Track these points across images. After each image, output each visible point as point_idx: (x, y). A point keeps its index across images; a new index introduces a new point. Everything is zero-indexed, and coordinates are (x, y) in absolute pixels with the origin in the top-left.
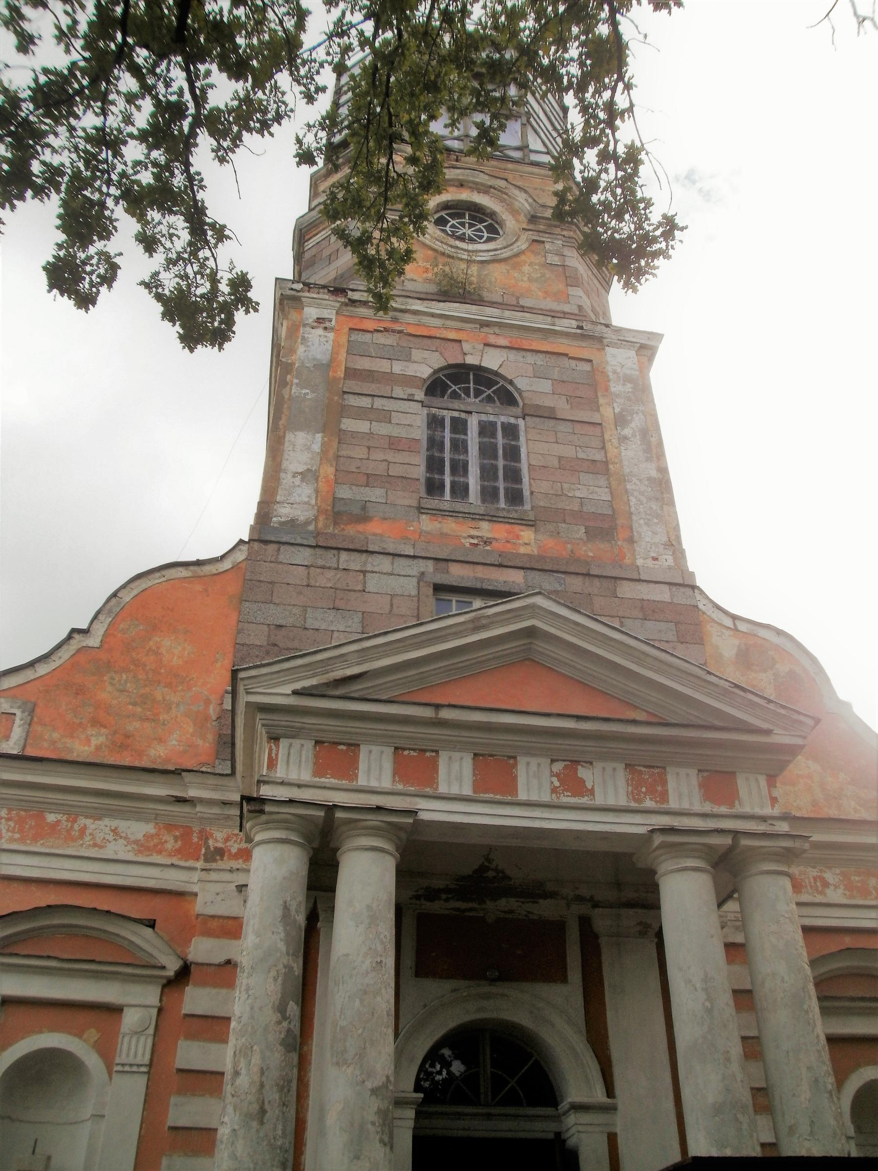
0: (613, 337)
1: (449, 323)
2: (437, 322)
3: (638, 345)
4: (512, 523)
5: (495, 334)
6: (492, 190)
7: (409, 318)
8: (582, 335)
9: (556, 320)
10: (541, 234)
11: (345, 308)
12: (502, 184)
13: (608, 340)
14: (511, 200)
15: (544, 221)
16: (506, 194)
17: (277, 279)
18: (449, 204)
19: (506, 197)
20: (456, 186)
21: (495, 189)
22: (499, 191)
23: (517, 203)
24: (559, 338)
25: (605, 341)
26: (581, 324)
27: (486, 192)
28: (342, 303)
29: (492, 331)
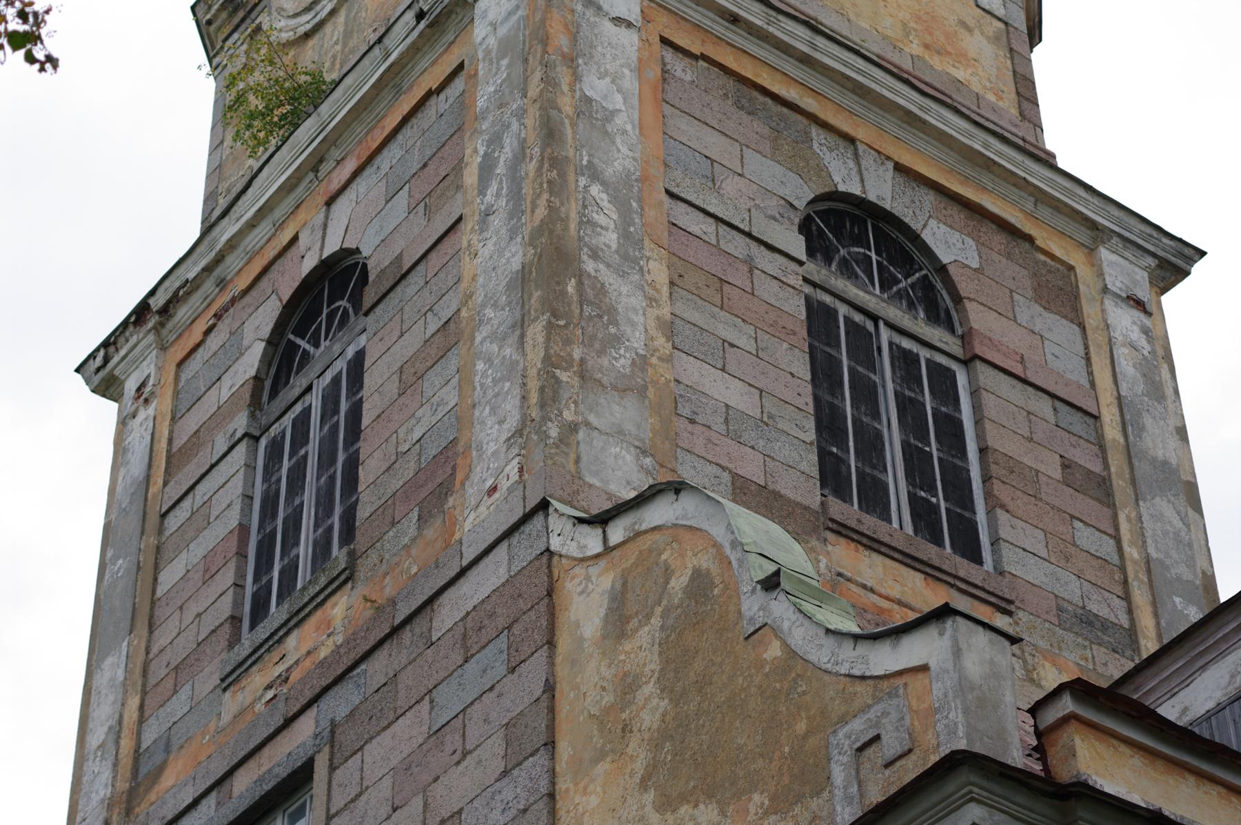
1: (279, 213)
2: (264, 229)
4: (983, 589)
5: (338, 162)
7: (233, 262)
8: (430, 26)
9: (386, 40)
11: (164, 332)
17: (77, 370)
20: (980, 167)
26: (416, 8)
28: (154, 328)
29: (332, 164)
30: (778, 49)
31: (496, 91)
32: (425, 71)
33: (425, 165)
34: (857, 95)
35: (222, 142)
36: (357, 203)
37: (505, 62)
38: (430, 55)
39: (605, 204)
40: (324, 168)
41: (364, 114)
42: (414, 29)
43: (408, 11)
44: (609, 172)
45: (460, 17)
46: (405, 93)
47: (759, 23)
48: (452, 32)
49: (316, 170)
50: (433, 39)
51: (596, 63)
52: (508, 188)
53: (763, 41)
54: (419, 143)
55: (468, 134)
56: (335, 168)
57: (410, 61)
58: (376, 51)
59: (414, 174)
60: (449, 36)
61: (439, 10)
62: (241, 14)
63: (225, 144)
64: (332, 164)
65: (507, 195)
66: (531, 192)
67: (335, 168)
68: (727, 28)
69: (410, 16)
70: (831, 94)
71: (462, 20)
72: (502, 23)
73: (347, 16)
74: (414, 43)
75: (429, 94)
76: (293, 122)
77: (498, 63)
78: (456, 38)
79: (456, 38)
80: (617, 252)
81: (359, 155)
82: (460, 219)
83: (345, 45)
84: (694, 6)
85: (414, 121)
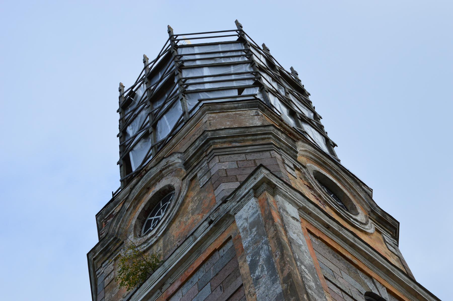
0: (234, 204)
3: (252, 191)
5: (171, 284)
6: (163, 172)
9: (195, 234)
10: (193, 171)
12: (163, 163)
13: (232, 210)
14: (174, 166)
15: (193, 159)
16: (170, 166)
18: (146, 209)
19: (171, 168)
21: (163, 169)
22: (166, 168)
23: (177, 165)
24: (206, 244)
25: (231, 213)
26: (209, 220)
27: (162, 177)
29: (168, 285)
30: (343, 240)
31: (252, 239)
32: (211, 244)
33: (217, 274)
34: (369, 261)
35: (104, 297)
36: (182, 296)
37: (254, 230)
38: (214, 237)
39: (307, 272)
40: (164, 288)
41: (184, 264)
42: (207, 228)
43: (205, 222)
44: (305, 263)
45: (228, 221)
46: (202, 253)
47: (337, 229)
48: (224, 227)
49: (161, 288)
50: (215, 231)
51: (291, 229)
52: (267, 267)
53: (338, 237)
54: (212, 268)
55: (239, 258)
56: (169, 287)
57: (205, 241)
58: (191, 238)
59: (212, 279)
60: (222, 229)
61: (219, 219)
62: (109, 254)
63: (106, 298)
64: (168, 285)
65: (267, 270)
66: (279, 266)
67: (169, 287)
68: (326, 230)
69: (206, 224)
70: (362, 260)
71: (228, 222)
72: (250, 218)
73: (164, 241)
74: (208, 233)
75: (215, 251)
76: (145, 276)
77: (251, 230)
78: (225, 230)
79: (225, 230)
80: (316, 289)
81: (182, 279)
82: (242, 285)
83: (164, 250)
84: (315, 220)
85: (208, 262)
